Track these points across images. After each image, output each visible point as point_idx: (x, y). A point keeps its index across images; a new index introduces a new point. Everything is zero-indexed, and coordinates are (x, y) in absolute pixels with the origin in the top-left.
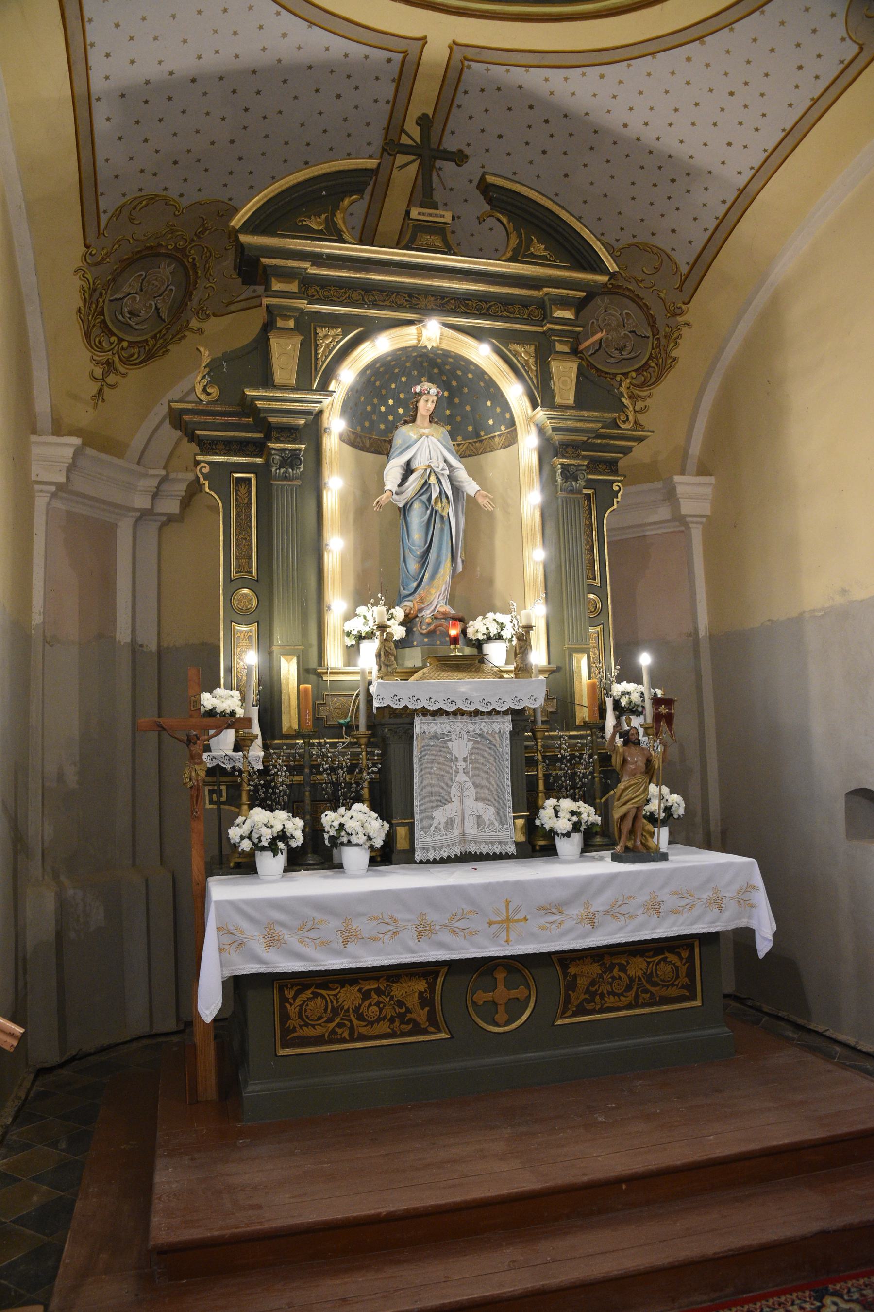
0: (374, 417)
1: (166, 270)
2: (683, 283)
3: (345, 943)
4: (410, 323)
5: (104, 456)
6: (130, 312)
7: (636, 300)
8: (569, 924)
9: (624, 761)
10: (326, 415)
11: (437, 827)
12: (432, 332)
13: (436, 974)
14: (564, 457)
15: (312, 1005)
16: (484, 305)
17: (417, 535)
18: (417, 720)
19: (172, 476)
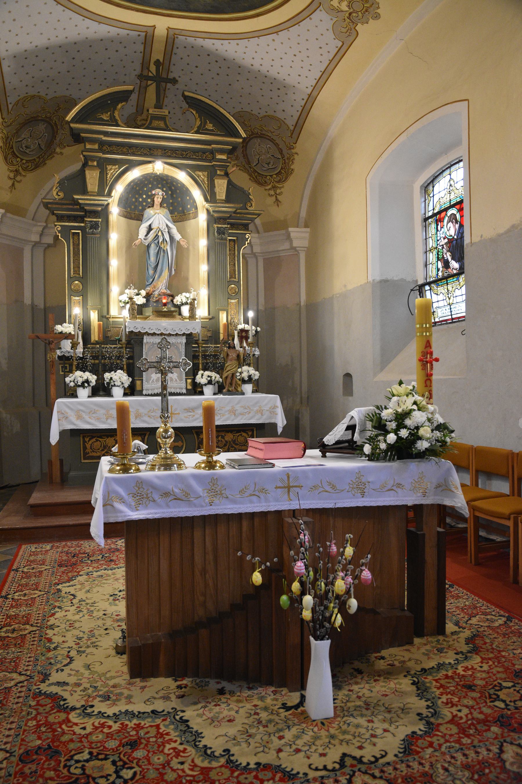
0: (136, 204)
1: (42, 127)
2: (292, 134)
3: (107, 419)
4: (150, 162)
6: (26, 147)
7: (272, 140)
8: (197, 416)
9: (228, 355)
10: (110, 206)
11: (153, 381)
12: (159, 167)
13: (145, 435)
14: (219, 224)
15: (95, 444)
16: (184, 153)
17: (153, 258)
18: (145, 337)
19: (49, 225)
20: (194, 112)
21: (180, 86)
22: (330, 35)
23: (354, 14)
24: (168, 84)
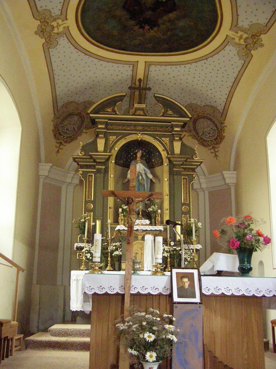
5: (58, 168)
6: (66, 129)
7: (210, 120)
16: (155, 128)
20: (161, 105)
21: (152, 91)
22: (237, 58)
23: (249, 46)
24: (147, 91)
